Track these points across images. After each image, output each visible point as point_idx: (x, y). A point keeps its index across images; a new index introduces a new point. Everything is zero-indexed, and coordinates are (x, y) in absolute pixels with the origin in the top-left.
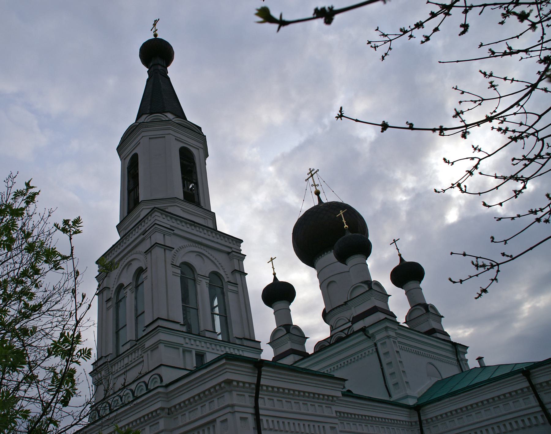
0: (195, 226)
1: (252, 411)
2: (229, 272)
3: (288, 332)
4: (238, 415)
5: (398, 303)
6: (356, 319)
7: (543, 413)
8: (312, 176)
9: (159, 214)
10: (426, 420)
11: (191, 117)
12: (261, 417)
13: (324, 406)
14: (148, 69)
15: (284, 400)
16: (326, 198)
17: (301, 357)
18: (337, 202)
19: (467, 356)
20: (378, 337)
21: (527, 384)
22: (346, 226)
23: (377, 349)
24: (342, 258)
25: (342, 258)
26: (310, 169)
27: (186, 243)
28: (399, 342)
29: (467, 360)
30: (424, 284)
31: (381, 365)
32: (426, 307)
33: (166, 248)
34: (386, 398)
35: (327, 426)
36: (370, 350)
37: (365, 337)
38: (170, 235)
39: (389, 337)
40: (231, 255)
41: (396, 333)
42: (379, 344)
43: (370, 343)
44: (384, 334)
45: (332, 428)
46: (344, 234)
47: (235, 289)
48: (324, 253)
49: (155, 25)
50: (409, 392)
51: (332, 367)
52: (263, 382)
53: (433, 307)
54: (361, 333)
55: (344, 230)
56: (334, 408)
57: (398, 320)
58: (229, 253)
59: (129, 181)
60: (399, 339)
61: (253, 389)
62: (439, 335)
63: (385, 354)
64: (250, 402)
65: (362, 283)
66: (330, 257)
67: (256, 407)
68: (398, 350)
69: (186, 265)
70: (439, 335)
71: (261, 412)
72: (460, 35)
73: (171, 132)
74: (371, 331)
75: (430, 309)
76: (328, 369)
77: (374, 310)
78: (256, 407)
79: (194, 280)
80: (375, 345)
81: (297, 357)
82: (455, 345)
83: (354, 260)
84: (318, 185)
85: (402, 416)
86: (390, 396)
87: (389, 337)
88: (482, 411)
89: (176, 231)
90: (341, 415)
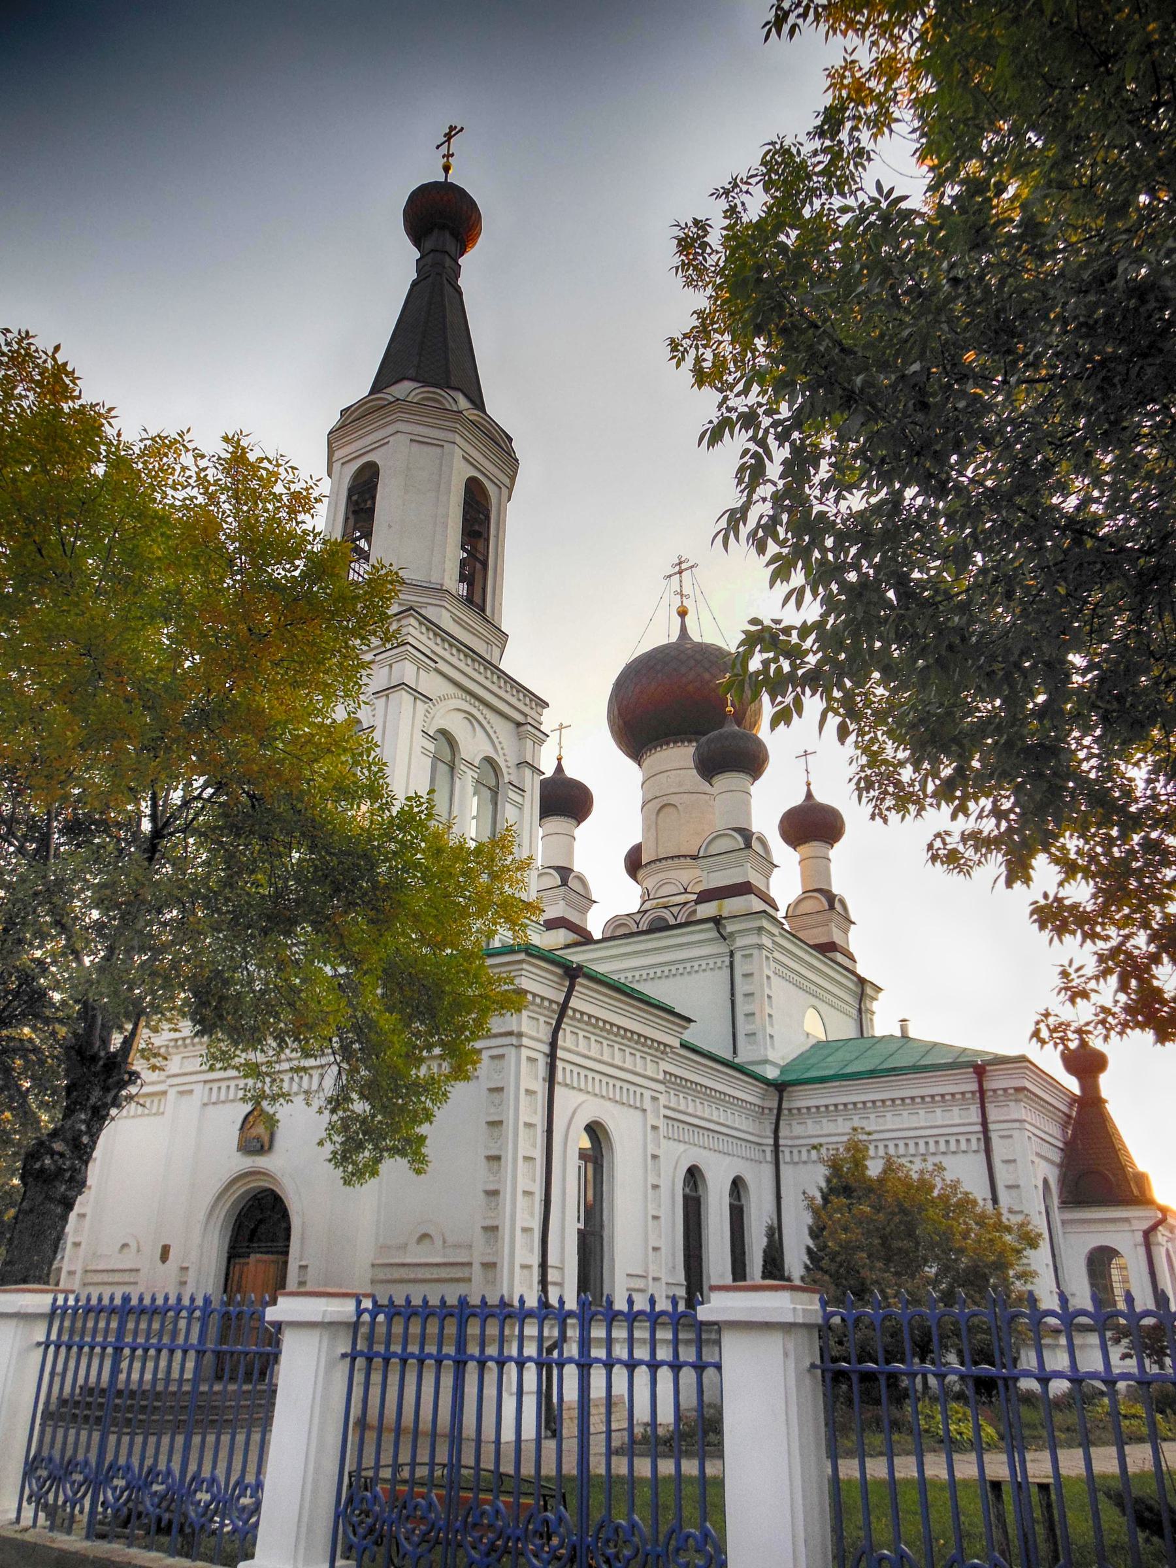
0: (473, 660)
2: (513, 761)
3: (564, 883)
5: (786, 882)
6: (706, 896)
7: (981, 1136)
8: (680, 572)
9: (416, 624)
10: (790, 1110)
11: (498, 407)
12: (558, 1063)
13: (649, 1058)
14: (418, 255)
15: (593, 1038)
17: (579, 939)
18: (719, 649)
20: (740, 942)
21: (974, 1087)
23: (732, 963)
24: (709, 767)
26: (680, 557)
27: (451, 689)
28: (776, 960)
29: (873, 1013)
30: (837, 853)
31: (733, 995)
32: (831, 898)
33: (419, 695)
34: (727, 1055)
35: (648, 1094)
36: (719, 961)
37: (715, 934)
38: (428, 671)
40: (522, 729)
41: (774, 942)
42: (738, 957)
43: (722, 948)
45: (654, 1099)
46: (721, 725)
47: (518, 799)
48: (668, 744)
49: (449, 137)
50: (772, 1055)
51: (637, 974)
52: (573, 1003)
54: (711, 925)
56: (664, 1066)
58: (519, 725)
59: (347, 519)
60: (777, 955)
61: (554, 1011)
62: (839, 957)
63: (745, 975)
64: (545, 1033)
65: (733, 829)
67: (553, 1045)
68: (771, 974)
69: (445, 734)
70: (839, 957)
73: (458, 439)
74: (730, 928)
75: (837, 905)
76: (629, 975)
77: (745, 889)
78: (553, 1045)
79: (452, 769)
80: (732, 954)
81: (572, 937)
82: (862, 981)
83: (726, 781)
84: (688, 596)
85: (749, 1094)
86: (735, 1052)
87: (760, 947)
88: (889, 1115)
89: (442, 666)
90: (672, 1081)
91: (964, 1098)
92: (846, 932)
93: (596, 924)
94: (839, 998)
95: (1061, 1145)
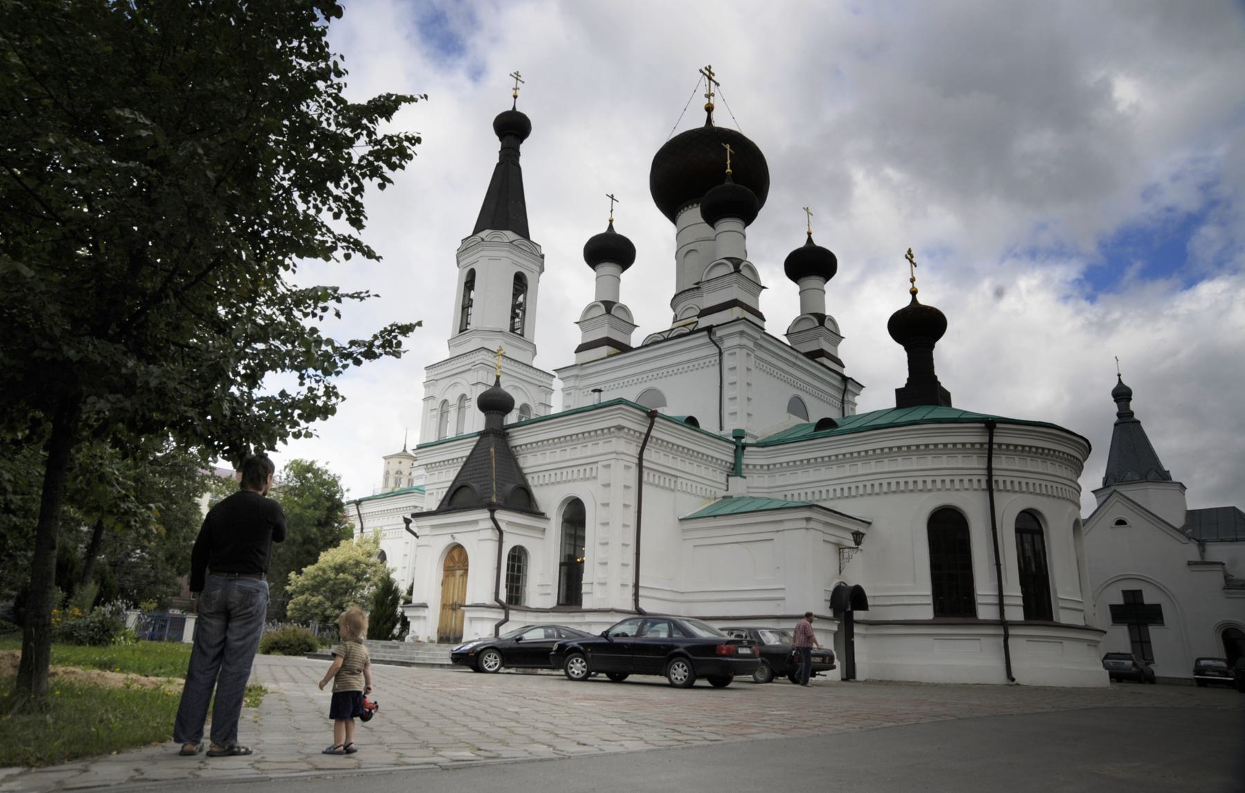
1: (636, 461)
4: (600, 464)
6: (704, 313)
16: (720, 121)
19: (857, 399)
22: (729, 170)
24: (711, 217)
25: (711, 217)
32: (821, 318)
36: (712, 359)
39: (741, 347)
42: (725, 356)
44: (736, 341)
53: (832, 321)
55: (726, 175)
57: (770, 327)
66: (693, 214)
67: (640, 459)
71: (645, 463)
72: (378, 258)
78: (640, 459)
82: (845, 379)
86: (721, 428)
91: (603, 434)
92: (756, 296)
93: (636, 340)
94: (814, 387)
95: (344, 725)
